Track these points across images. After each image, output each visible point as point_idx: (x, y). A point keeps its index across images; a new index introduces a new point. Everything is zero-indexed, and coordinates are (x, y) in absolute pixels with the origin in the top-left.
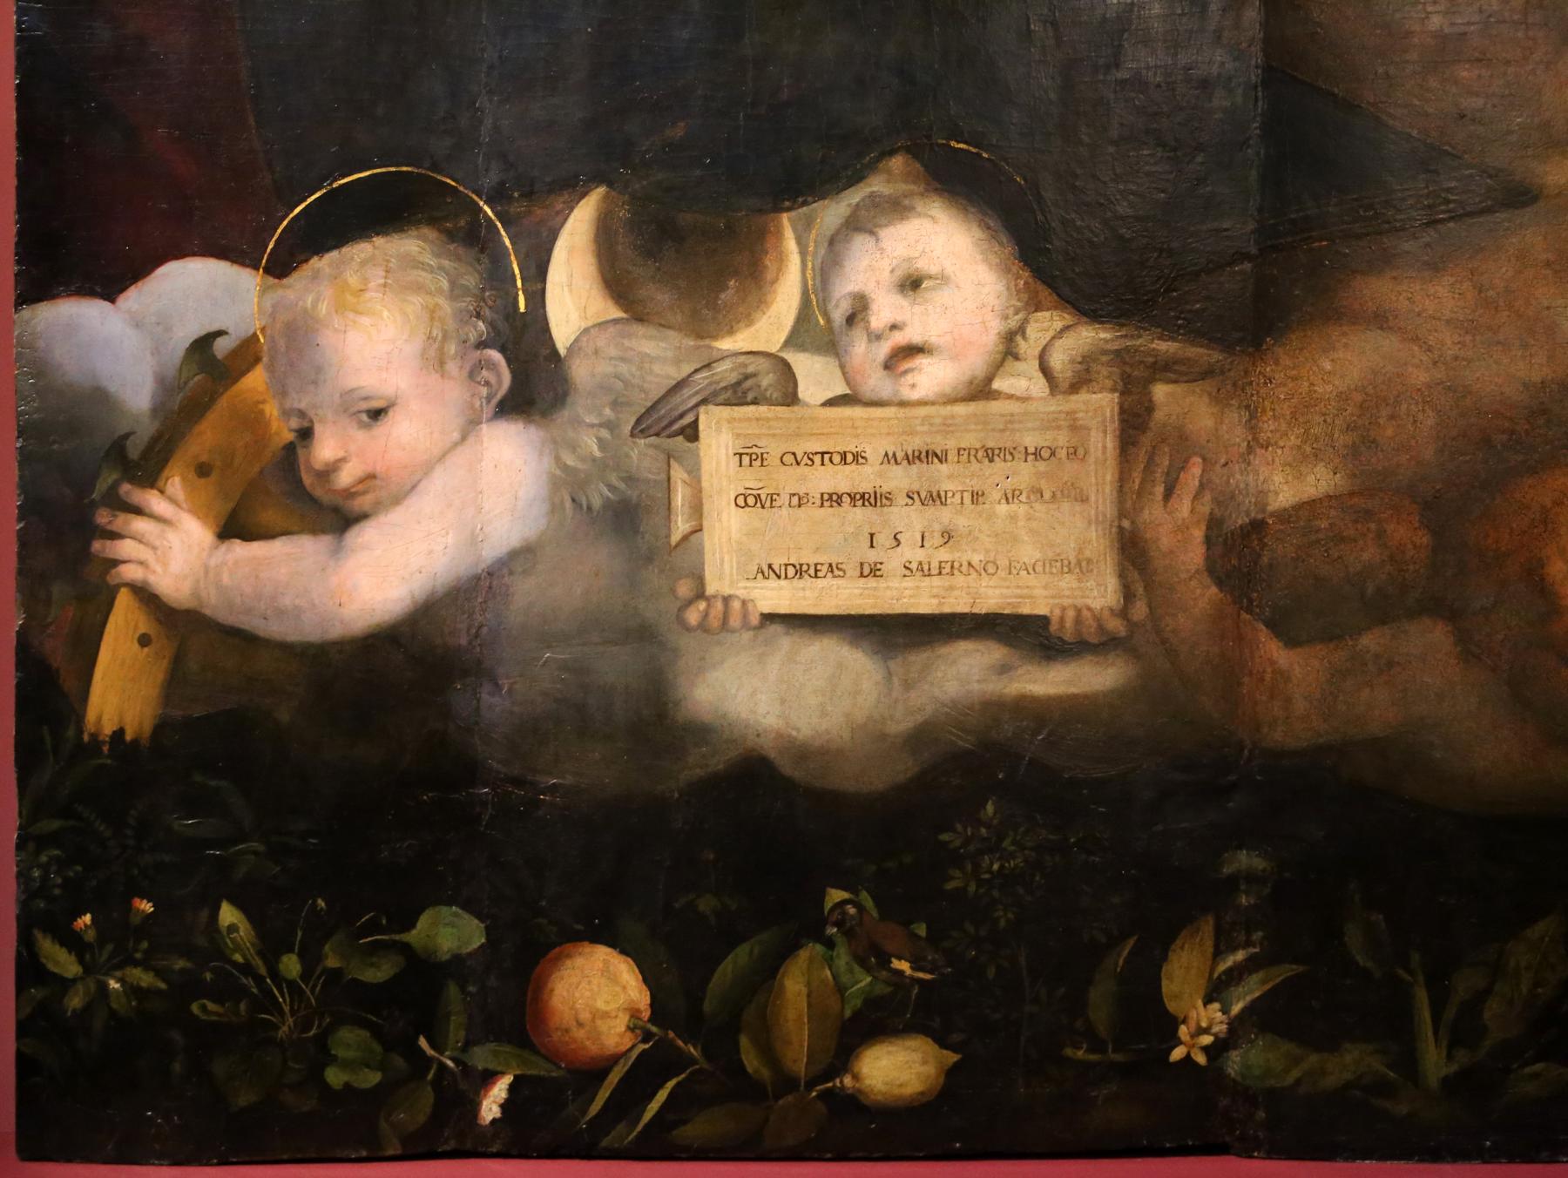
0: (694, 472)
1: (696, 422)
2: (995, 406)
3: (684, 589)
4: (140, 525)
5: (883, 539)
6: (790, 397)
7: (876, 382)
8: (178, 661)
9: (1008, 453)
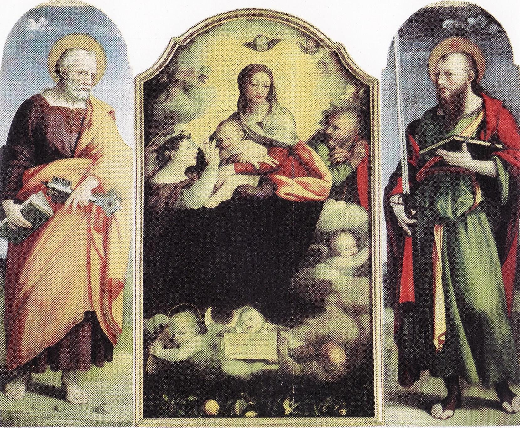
0: (223, 341)
1: (224, 335)
2: (262, 334)
3: (223, 356)
4: (152, 347)
5: (248, 350)
6: (236, 332)
7: (246, 330)
8: (158, 364)
9: (263, 340)
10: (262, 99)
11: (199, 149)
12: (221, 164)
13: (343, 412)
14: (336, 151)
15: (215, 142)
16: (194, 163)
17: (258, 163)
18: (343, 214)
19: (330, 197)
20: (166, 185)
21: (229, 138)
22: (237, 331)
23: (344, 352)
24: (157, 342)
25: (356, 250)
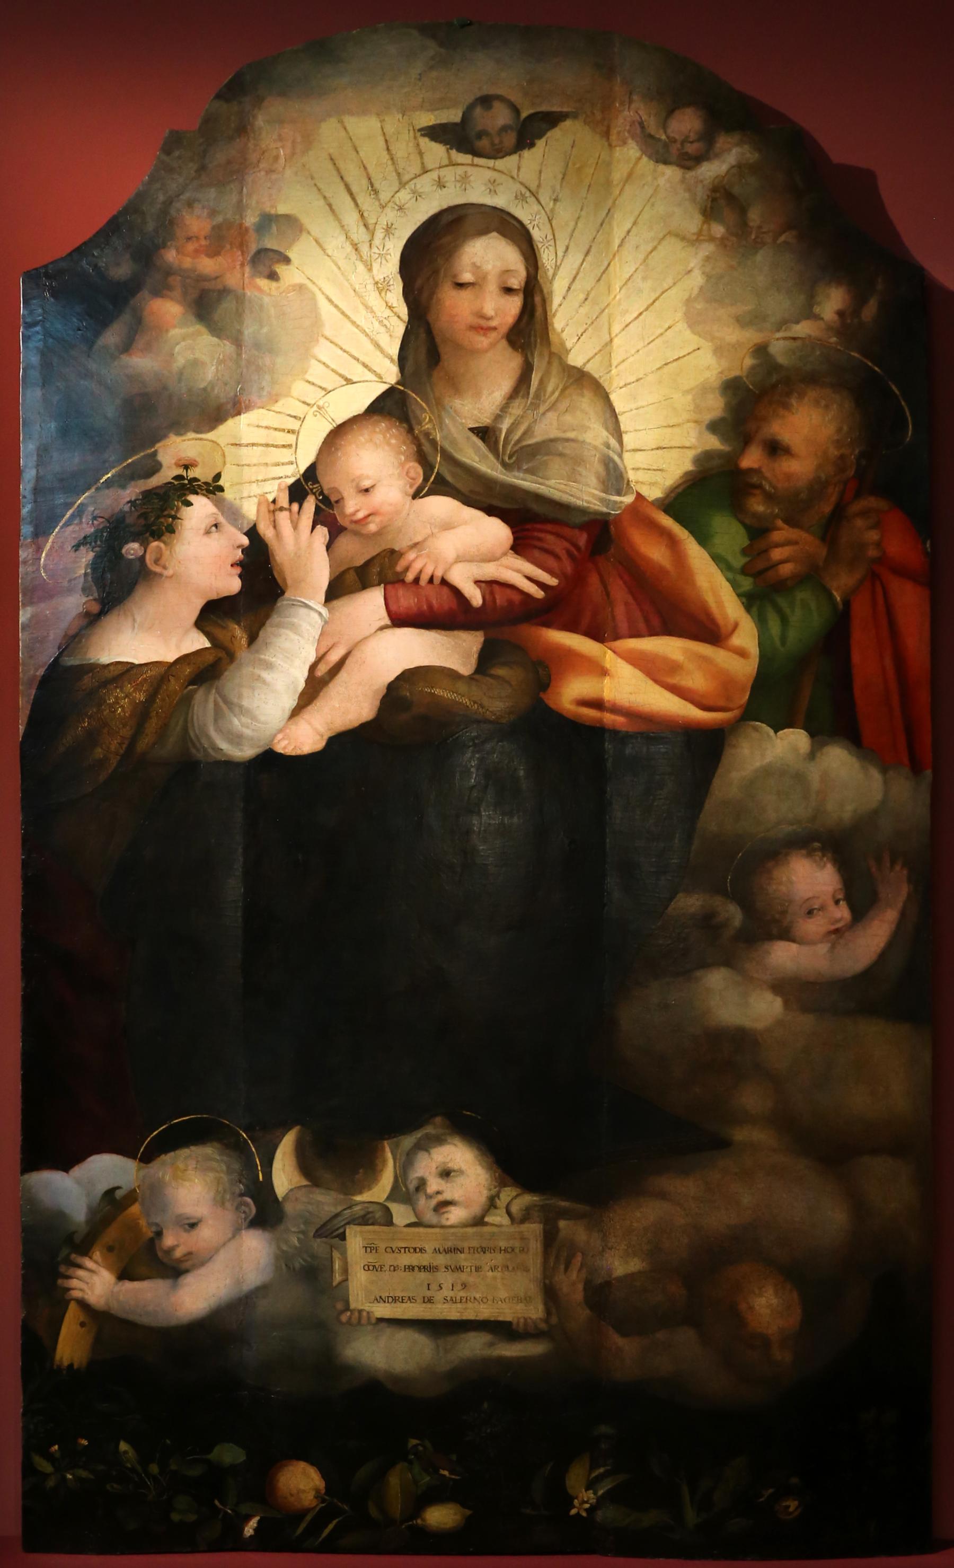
0: (344, 1254)
1: (344, 1233)
2: (486, 1229)
3: (340, 1306)
4: (81, 1273)
5: (434, 1287)
6: (389, 1222)
7: (430, 1217)
10: (493, 335)
11: (252, 533)
12: (336, 591)
13: (791, 1509)
14: (777, 536)
15: (310, 505)
16: (233, 585)
17: (477, 582)
18: (800, 778)
19: (750, 714)
20: (128, 670)
21: (367, 490)
22: (396, 1220)
23: (795, 1295)
24: (243, 703)
25: (843, 913)
